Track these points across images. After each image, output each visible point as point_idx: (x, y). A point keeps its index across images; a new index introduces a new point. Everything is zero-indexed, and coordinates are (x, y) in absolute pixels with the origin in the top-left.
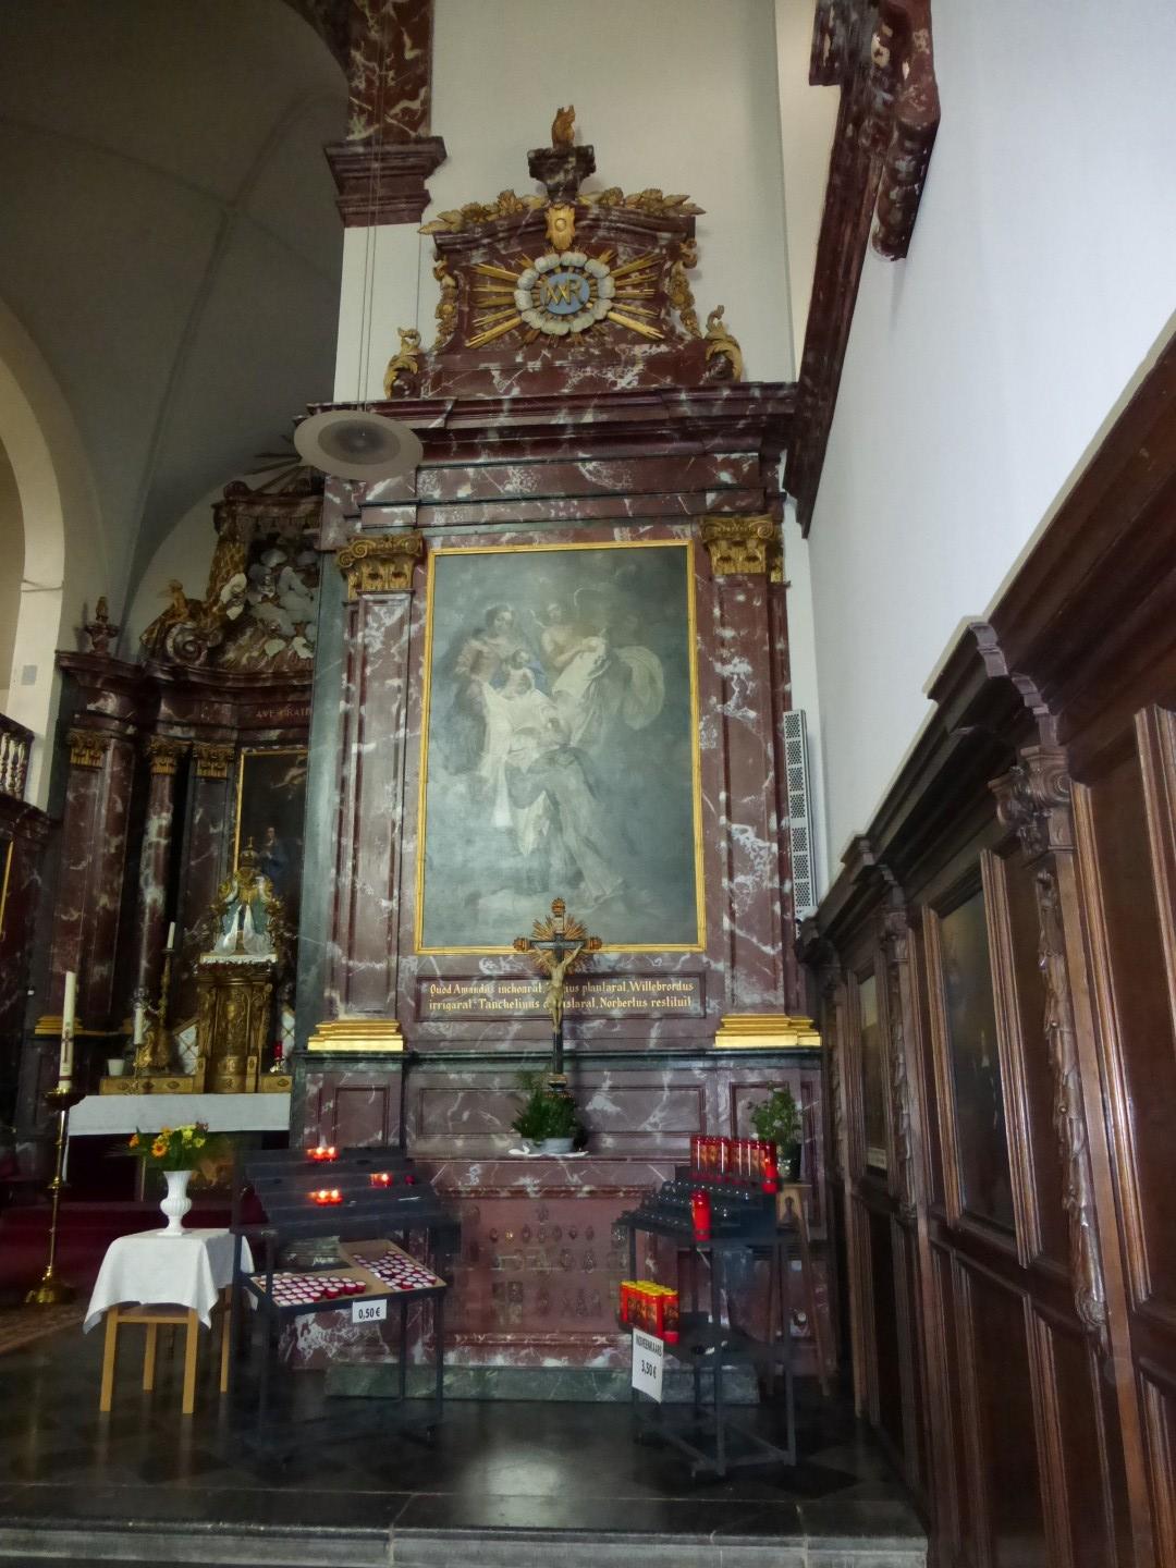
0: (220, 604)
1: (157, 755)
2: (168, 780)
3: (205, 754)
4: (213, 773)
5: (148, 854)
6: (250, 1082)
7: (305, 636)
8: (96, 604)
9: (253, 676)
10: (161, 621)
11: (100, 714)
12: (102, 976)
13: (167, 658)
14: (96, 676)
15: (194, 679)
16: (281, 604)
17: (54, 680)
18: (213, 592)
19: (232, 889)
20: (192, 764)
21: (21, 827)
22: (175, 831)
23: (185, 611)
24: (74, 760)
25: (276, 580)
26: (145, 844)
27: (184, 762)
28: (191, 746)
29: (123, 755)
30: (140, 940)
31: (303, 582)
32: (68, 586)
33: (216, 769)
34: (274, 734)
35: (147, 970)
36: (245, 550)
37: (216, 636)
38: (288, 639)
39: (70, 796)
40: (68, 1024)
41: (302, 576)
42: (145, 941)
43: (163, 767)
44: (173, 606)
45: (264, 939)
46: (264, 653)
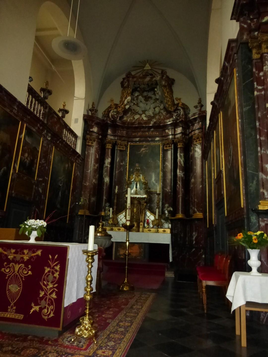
0: (124, 104)
1: (108, 143)
2: (110, 150)
3: (119, 144)
4: (122, 149)
5: (105, 169)
6: (141, 229)
7: (145, 114)
8: (92, 104)
9: (133, 124)
10: (108, 109)
11: (93, 132)
12: (93, 201)
13: (110, 119)
14: (93, 121)
15: (118, 124)
16: (139, 106)
17: (83, 121)
18: (122, 101)
19: (133, 178)
20: (116, 146)
21: (76, 159)
22: (112, 163)
23: (114, 107)
24: (87, 143)
25: (137, 100)
26: (104, 166)
27: (114, 145)
28: (116, 142)
29: (99, 143)
30: (103, 191)
31: (145, 100)
32: (86, 98)
33: (122, 148)
34: (137, 139)
35: (105, 199)
36: (131, 90)
37: (121, 114)
38: (141, 115)
39: (86, 153)
40: (129, 204)
41: (144, 98)
42: (105, 191)
43: (109, 146)
44: (111, 105)
45: (142, 191)
46: (134, 118)
